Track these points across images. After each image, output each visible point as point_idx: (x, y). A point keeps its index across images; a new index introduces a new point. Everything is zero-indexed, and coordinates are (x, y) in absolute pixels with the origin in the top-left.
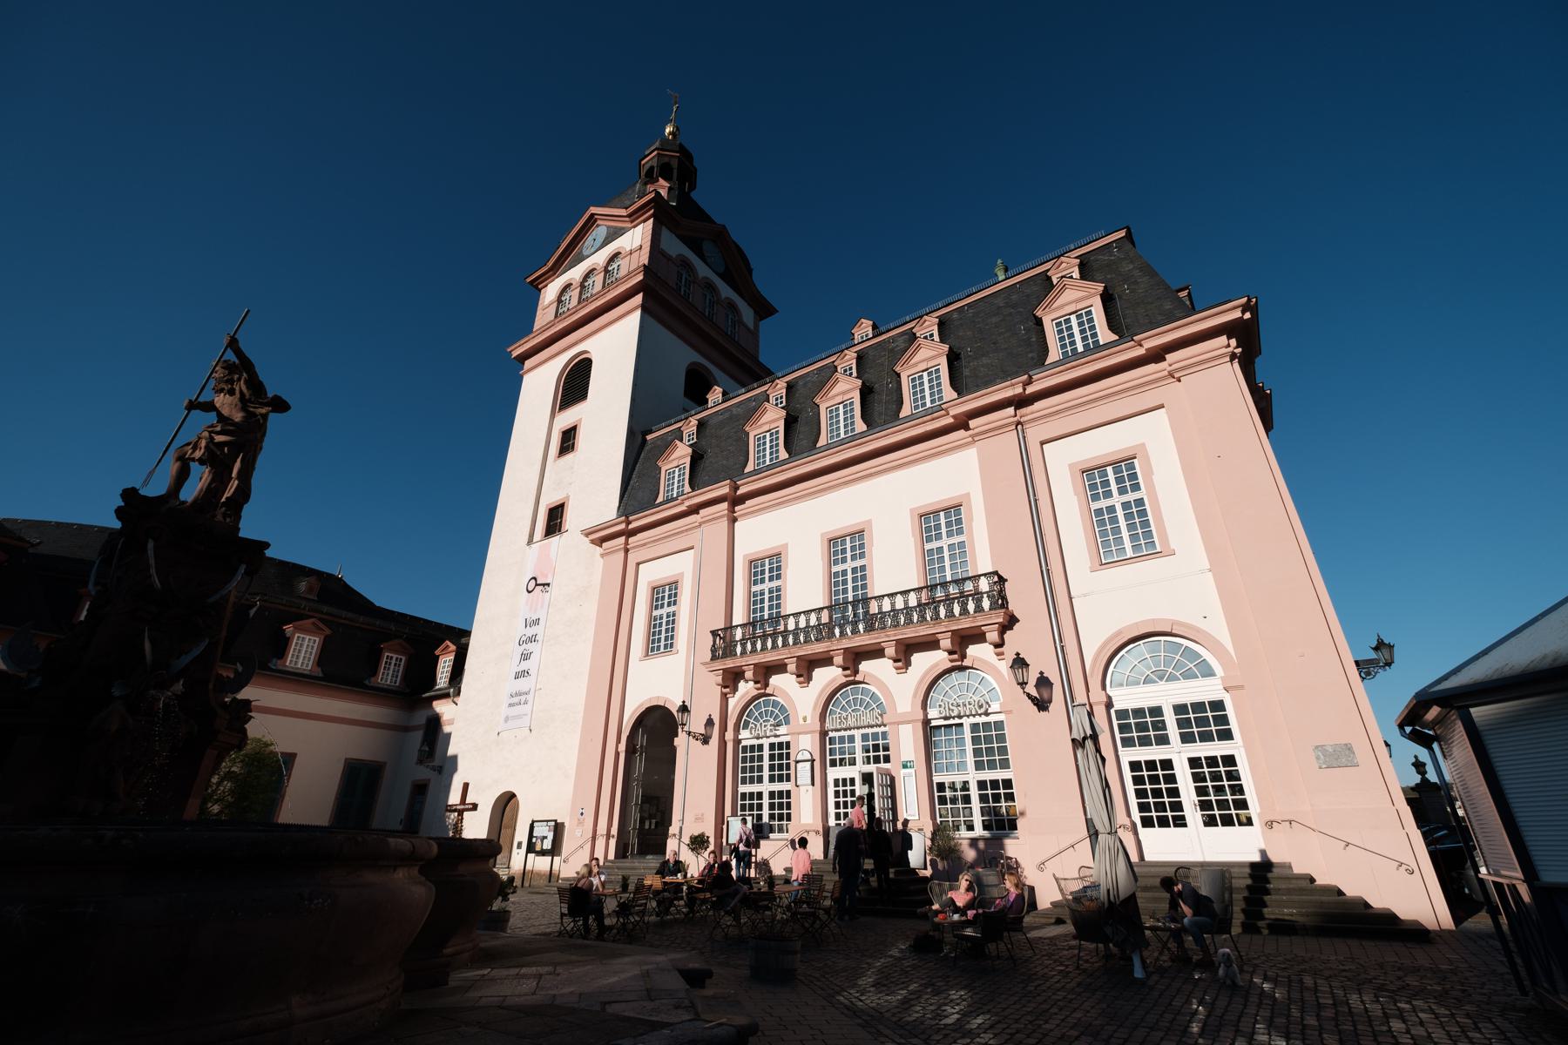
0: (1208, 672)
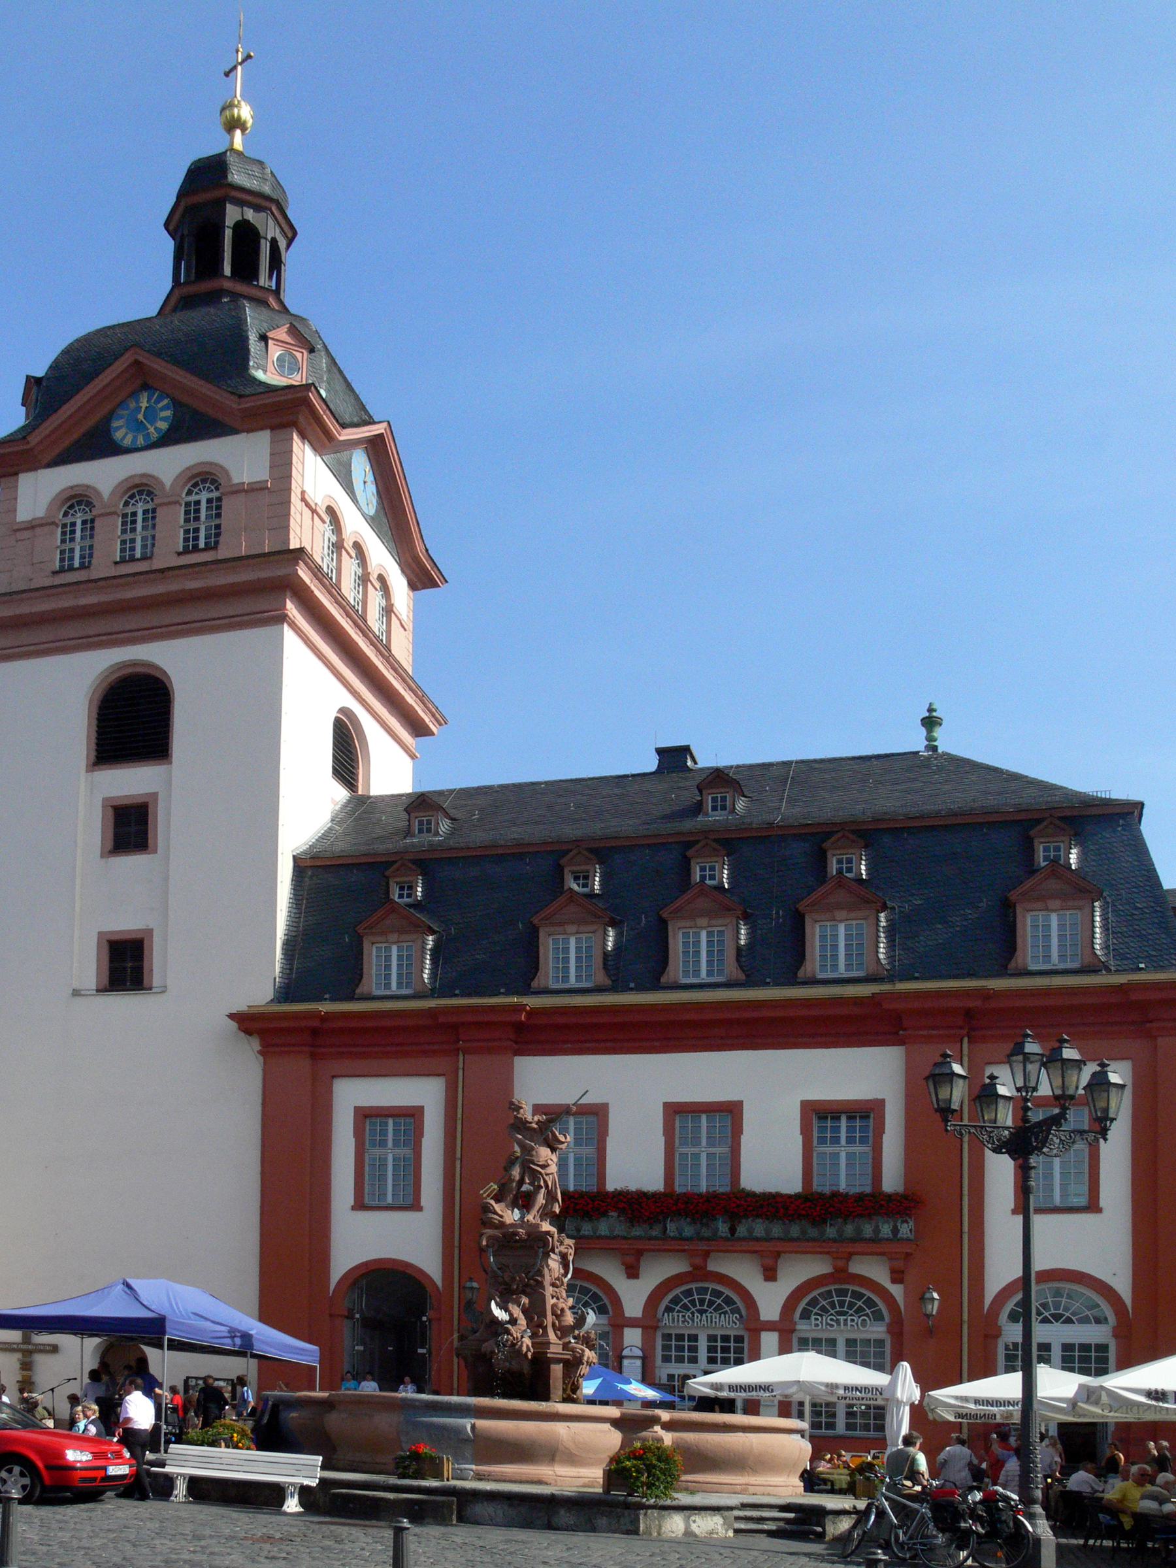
0: (878, 1316)
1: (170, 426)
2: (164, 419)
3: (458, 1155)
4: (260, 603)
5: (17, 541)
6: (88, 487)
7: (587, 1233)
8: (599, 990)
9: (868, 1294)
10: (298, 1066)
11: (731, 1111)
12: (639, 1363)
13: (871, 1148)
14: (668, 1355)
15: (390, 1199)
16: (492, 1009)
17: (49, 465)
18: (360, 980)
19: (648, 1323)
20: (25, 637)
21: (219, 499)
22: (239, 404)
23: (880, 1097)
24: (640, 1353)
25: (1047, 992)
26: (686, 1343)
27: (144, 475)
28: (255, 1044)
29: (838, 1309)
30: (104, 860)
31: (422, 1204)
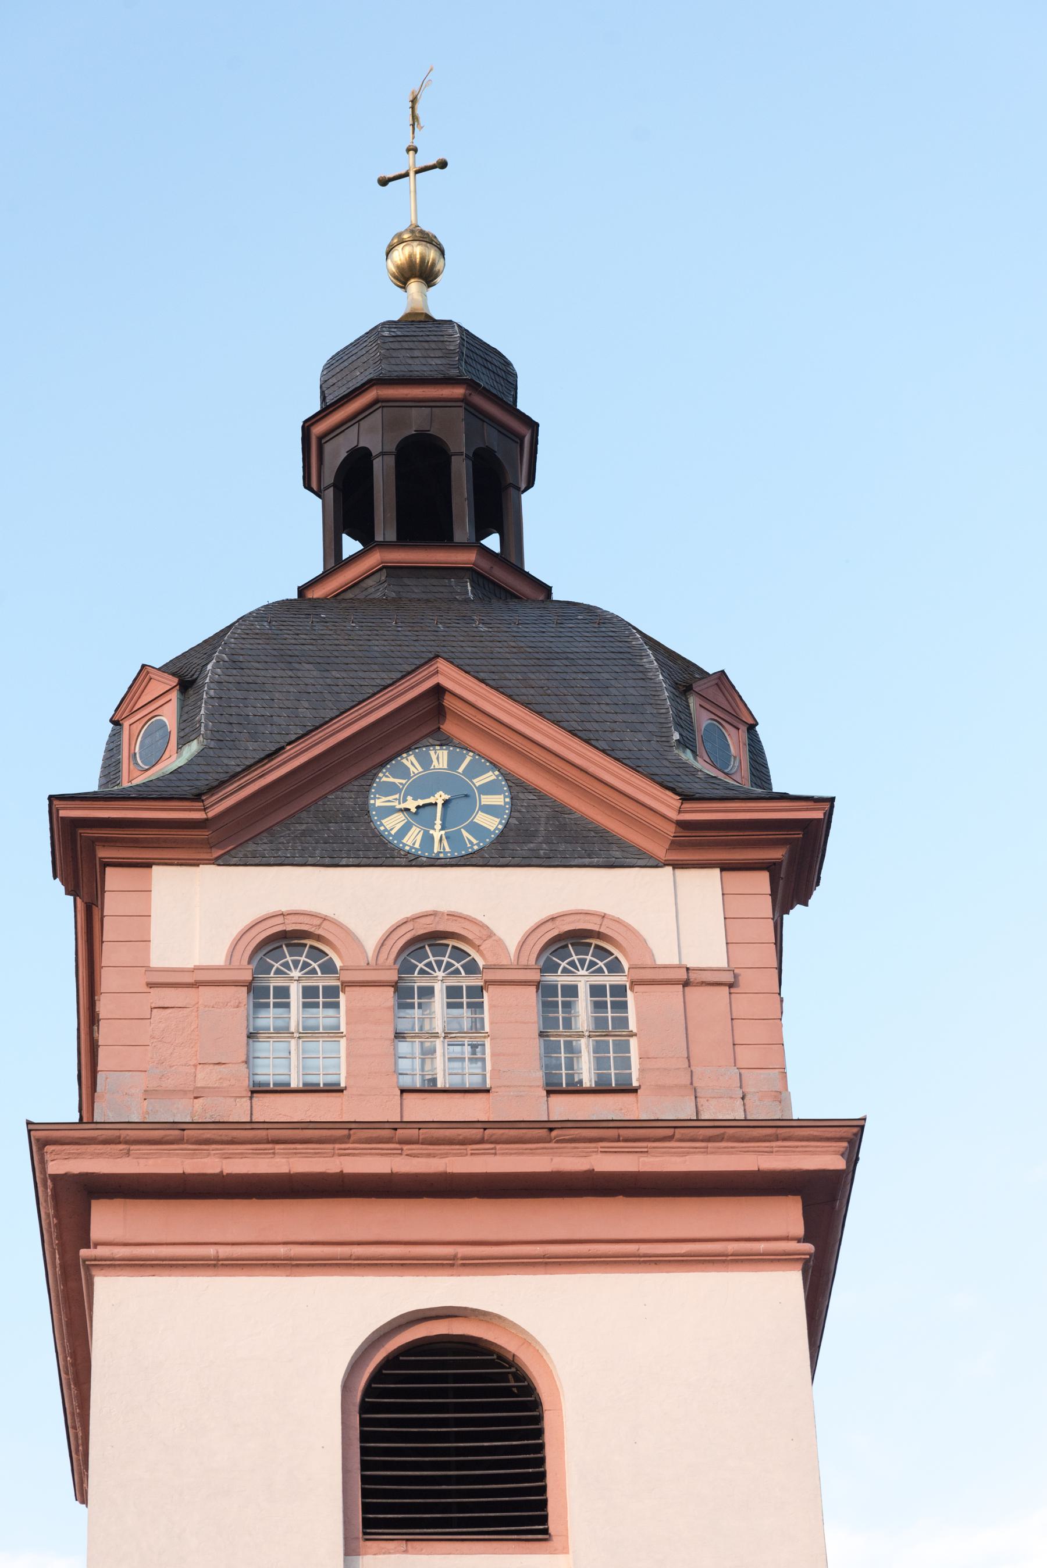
22: (680, 812)
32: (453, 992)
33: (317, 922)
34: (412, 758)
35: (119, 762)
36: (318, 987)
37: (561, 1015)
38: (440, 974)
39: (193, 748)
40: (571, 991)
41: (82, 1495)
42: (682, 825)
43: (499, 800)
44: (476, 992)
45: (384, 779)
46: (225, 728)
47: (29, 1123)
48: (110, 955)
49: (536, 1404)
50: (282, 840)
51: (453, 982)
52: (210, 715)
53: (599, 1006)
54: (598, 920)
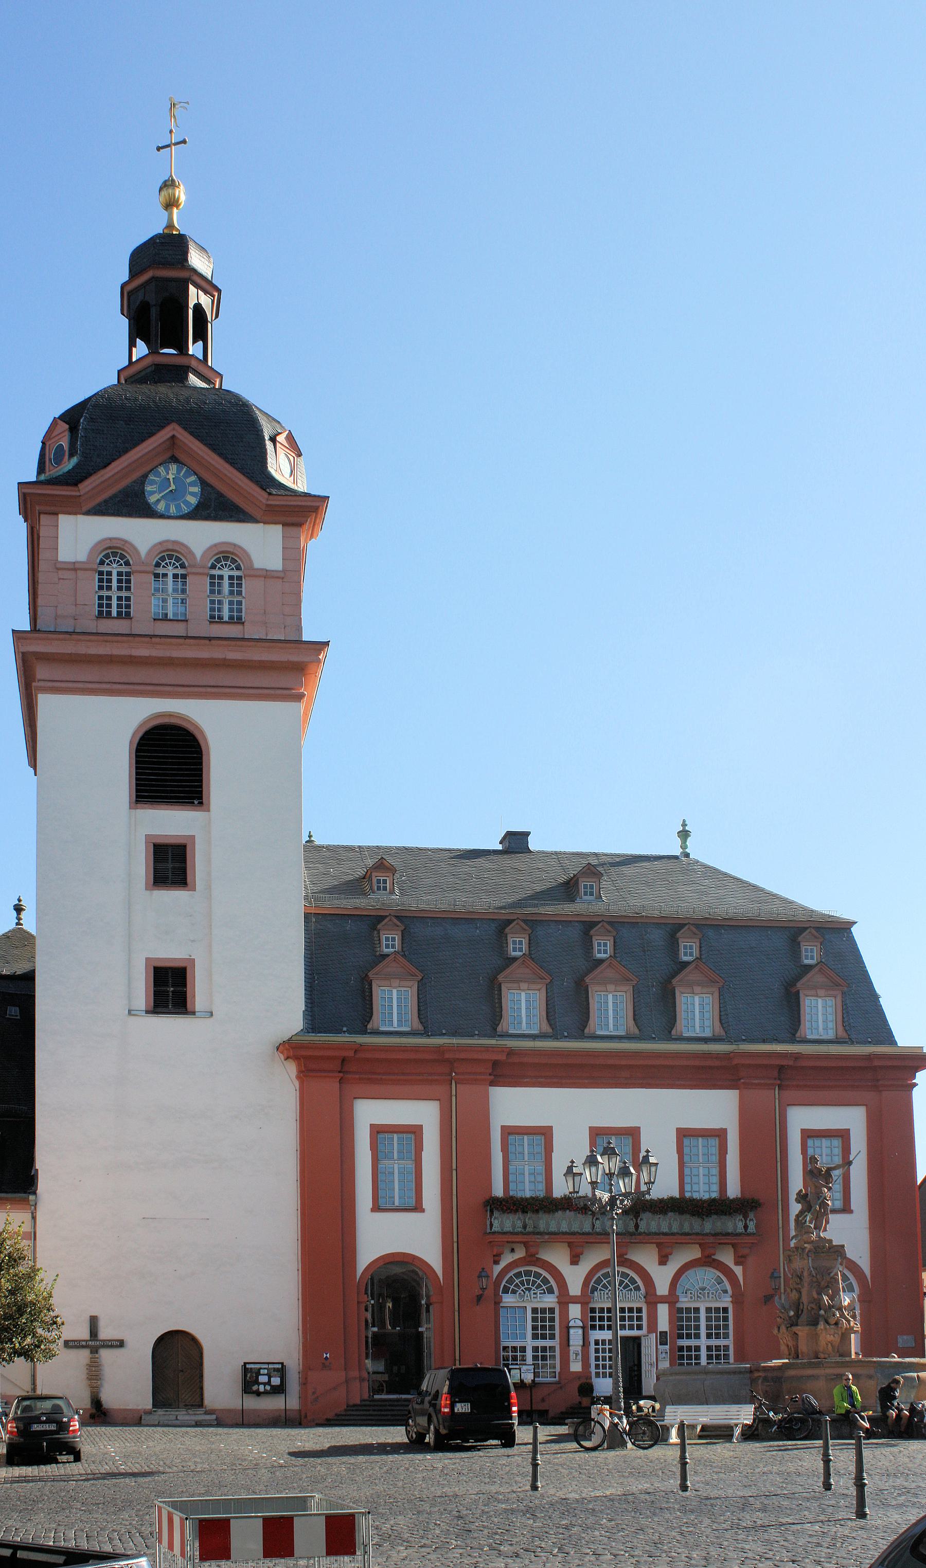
0: (550, 1291)
1: (199, 502)
2: (193, 494)
3: (454, 1167)
4: (283, 680)
5: (59, 579)
6: (126, 542)
7: (751, 1231)
8: (628, 1038)
9: (511, 1274)
10: (330, 1086)
11: (632, 1135)
12: (580, 1331)
13: (544, 1163)
14: (640, 1324)
15: (397, 1203)
16: (471, 1048)
17: (88, 513)
18: (371, 1017)
19: (583, 1300)
20: (116, 674)
21: (128, 574)
22: (267, 500)
23: (724, 1127)
24: (581, 1324)
25: (828, 1057)
26: (597, 1315)
27: (176, 542)
28: (292, 1068)
29: (526, 1286)
30: (148, 892)
31: (852, 1208)
32: (175, 576)
33: (123, 543)
34: (162, 468)
35: (44, 463)
36: (122, 597)
37: (216, 588)
38: (170, 568)
39: (75, 460)
40: (221, 577)
41: (33, 761)
42: (268, 505)
43: (196, 489)
44: (184, 576)
45: (151, 478)
46: (88, 451)
47: (13, 630)
48: (44, 555)
49: (199, 746)
50: (109, 505)
51: (176, 571)
52: (82, 445)
53: (231, 585)
54: (233, 547)
